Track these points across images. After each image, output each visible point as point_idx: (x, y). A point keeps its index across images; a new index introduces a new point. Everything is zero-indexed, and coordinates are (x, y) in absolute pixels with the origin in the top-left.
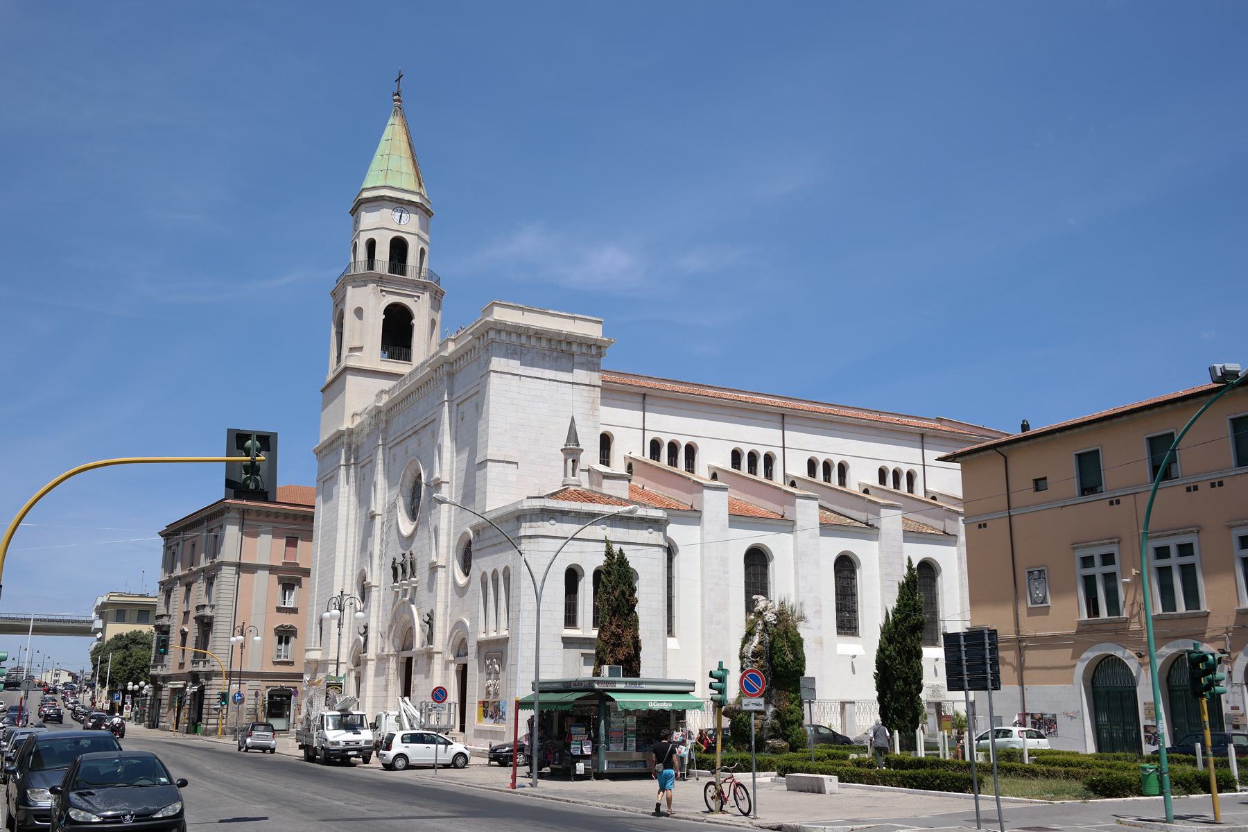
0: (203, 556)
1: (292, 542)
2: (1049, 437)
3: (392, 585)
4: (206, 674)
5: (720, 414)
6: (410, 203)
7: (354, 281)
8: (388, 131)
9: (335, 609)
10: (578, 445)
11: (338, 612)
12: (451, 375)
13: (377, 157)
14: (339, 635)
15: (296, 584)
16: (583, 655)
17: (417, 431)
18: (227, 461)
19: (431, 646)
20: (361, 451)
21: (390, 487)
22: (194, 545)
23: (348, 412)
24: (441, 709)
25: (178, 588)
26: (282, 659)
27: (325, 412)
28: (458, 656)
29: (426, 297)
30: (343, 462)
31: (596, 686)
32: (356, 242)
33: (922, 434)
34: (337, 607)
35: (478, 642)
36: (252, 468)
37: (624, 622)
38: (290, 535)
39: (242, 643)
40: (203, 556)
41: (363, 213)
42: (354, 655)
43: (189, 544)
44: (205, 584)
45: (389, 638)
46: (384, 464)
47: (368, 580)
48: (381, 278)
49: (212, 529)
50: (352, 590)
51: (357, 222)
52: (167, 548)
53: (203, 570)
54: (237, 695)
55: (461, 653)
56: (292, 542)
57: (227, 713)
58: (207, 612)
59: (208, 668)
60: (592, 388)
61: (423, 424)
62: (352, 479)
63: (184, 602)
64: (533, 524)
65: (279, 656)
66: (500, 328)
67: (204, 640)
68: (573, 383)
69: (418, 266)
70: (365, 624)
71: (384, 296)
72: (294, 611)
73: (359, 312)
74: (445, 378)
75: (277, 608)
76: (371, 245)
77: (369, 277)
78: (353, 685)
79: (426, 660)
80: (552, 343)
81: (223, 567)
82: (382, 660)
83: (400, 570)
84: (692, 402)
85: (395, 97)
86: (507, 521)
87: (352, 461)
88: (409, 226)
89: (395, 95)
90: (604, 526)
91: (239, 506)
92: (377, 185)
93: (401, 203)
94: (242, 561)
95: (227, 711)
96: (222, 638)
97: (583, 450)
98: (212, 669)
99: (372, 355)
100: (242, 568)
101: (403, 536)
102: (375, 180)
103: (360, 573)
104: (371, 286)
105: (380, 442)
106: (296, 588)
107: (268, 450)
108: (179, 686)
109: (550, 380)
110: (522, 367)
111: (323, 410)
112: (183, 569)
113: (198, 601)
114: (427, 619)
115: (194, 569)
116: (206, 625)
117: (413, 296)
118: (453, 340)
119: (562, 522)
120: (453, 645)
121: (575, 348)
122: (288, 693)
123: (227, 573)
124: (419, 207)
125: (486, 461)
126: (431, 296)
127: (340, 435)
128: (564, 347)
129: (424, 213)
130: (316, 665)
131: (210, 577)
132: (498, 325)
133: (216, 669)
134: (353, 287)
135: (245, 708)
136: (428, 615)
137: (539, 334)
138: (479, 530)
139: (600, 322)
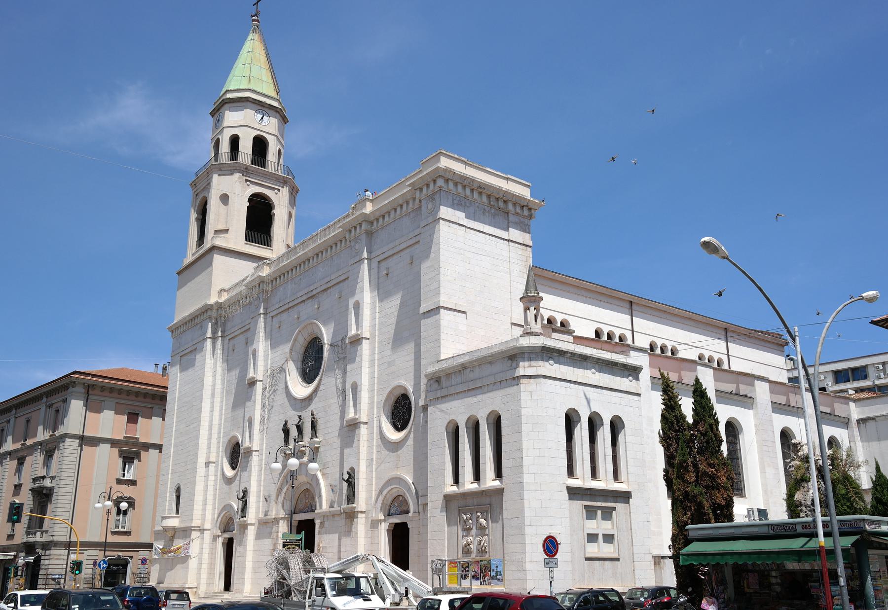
0: (40, 428)
1: (133, 418)
4: (43, 545)
5: (584, 296)
6: (271, 107)
7: (220, 170)
8: (248, 45)
12: (370, 234)
14: (108, 520)
15: (135, 457)
16: (586, 507)
17: (314, 295)
20: (229, 325)
21: (229, 370)
22: (28, 421)
23: (215, 288)
24: (553, 565)
25: (8, 463)
26: (120, 529)
27: (181, 291)
28: (225, 531)
29: (285, 191)
30: (209, 334)
31: (868, 528)
32: (218, 139)
33: (726, 329)
35: (445, 496)
37: (716, 461)
38: (131, 412)
40: (40, 428)
41: (227, 112)
42: (221, 521)
43: (22, 421)
44: (42, 456)
45: (276, 501)
46: (223, 350)
48: (246, 168)
49: (52, 404)
51: (219, 121)
53: (41, 443)
54: (102, 563)
56: (133, 418)
57: (65, 583)
58: (47, 483)
59: (46, 538)
60: (525, 248)
61: (323, 288)
62: (219, 352)
63: (15, 475)
64: (533, 363)
65: (117, 527)
66: (448, 177)
68: (509, 241)
69: (277, 162)
71: (248, 185)
72: (133, 483)
73: (225, 199)
75: (117, 480)
76: (235, 141)
77: (233, 166)
78: (219, 550)
79: (344, 520)
80: (491, 200)
81: (67, 439)
82: (266, 525)
83: (294, 433)
84: (564, 283)
85: (254, 18)
86: (490, 363)
87: (220, 334)
88: (269, 126)
89: (253, 17)
90: (593, 370)
91: (83, 381)
92: (241, 87)
93: (263, 106)
94: (85, 434)
95: (65, 580)
98: (51, 539)
99: (236, 238)
100: (84, 441)
101: (295, 399)
104: (237, 175)
105: (262, 311)
106: (136, 461)
108: (9, 558)
109: (490, 235)
110: (466, 219)
111: (178, 290)
112: (14, 442)
113: (33, 473)
115: (29, 442)
117: (274, 189)
118: (372, 201)
119: (559, 363)
120: (383, 503)
121: (510, 206)
122: (123, 562)
123: (71, 445)
124: (278, 112)
125: (438, 308)
126: (289, 191)
127: (207, 309)
128: (501, 204)
129: (281, 119)
130: (173, 533)
131: (49, 450)
132: (448, 174)
133: (55, 539)
134: (219, 175)
135: (83, 577)
137: (481, 188)
138: (440, 378)
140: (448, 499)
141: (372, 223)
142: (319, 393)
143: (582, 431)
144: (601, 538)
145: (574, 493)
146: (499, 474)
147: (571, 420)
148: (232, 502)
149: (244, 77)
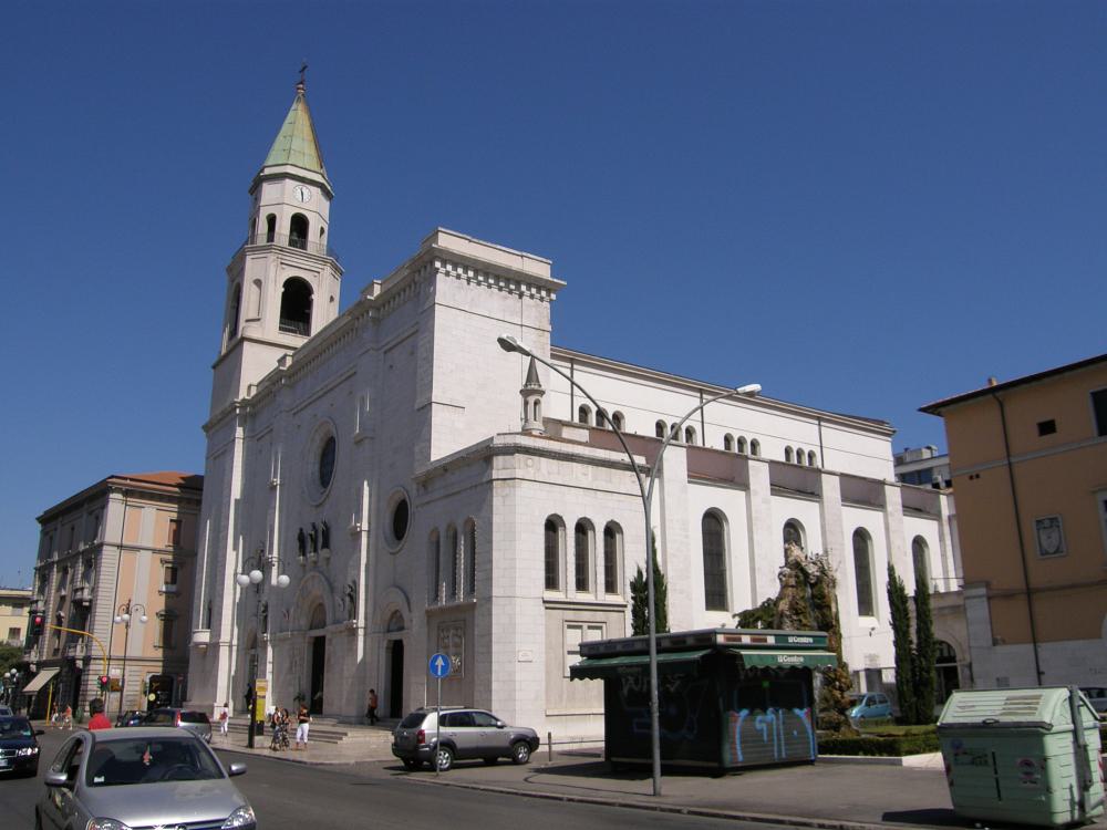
2: (1056, 377)
10: (540, 386)
12: (377, 321)
22: (73, 529)
51: (257, 199)
52: (44, 533)
55: (392, 627)
74: (371, 324)
76: (272, 220)
112: (85, 544)
140: (429, 614)
141: (378, 309)
143: (568, 541)
145: (550, 605)
147: (553, 525)
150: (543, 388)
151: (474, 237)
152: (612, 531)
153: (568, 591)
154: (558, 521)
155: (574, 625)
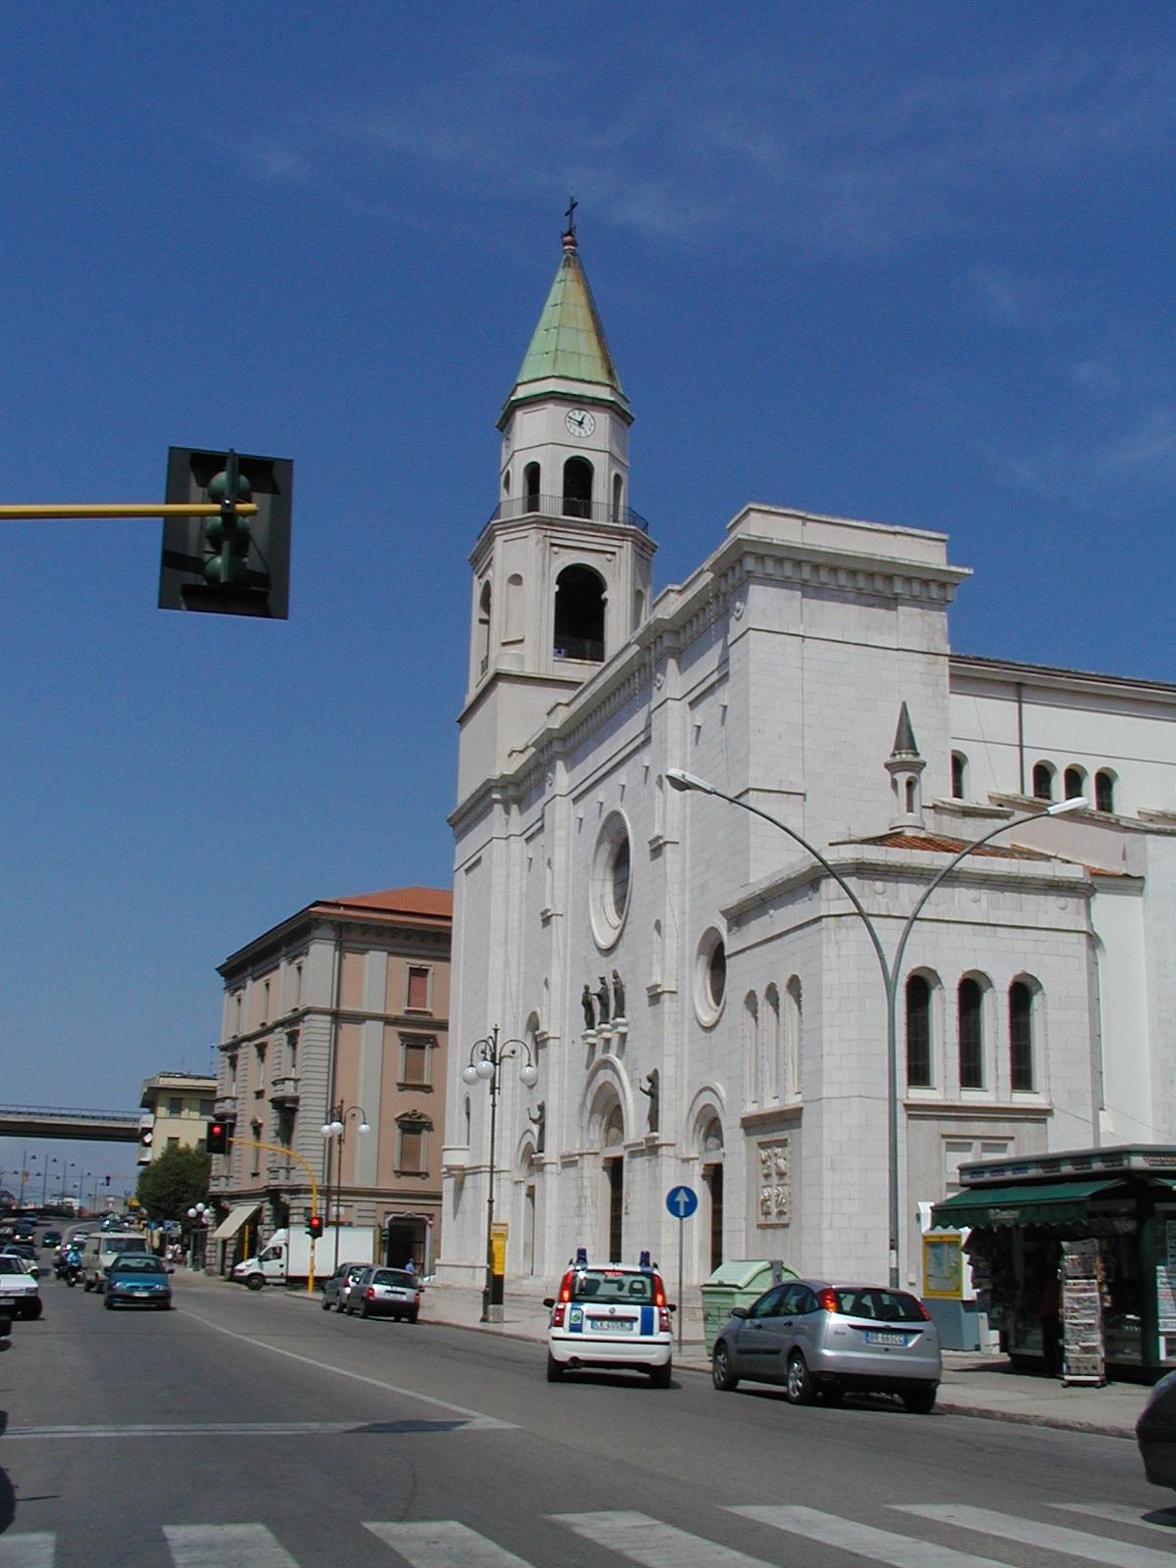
3: (583, 1033)
8: (556, 293)
9: (485, 1059)
10: (917, 754)
11: (491, 1064)
13: (540, 333)
18: (167, 516)
19: (655, 1134)
29: (626, 551)
34: (488, 1057)
36: (231, 533)
39: (340, 1136)
47: (543, 1028)
50: (513, 1031)
58: (288, 1089)
67: (286, 1132)
69: (612, 502)
70: (539, 1102)
76: (533, 472)
83: (597, 1007)
89: (566, 235)
96: (314, 1128)
97: (924, 765)
102: (536, 371)
103: (530, 1019)
107: (274, 490)
114: (647, 1086)
116: (286, 1109)
136: (650, 1080)
139: (943, 541)
142: (624, 938)
144: (311, 1282)
146: (1022, 1078)
148: (718, 1084)
149: (547, 353)
150: (922, 758)
151: (809, 511)
152: (1022, 994)
153: (945, 1086)
154: (929, 978)
155: (957, 1143)
